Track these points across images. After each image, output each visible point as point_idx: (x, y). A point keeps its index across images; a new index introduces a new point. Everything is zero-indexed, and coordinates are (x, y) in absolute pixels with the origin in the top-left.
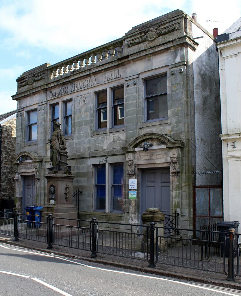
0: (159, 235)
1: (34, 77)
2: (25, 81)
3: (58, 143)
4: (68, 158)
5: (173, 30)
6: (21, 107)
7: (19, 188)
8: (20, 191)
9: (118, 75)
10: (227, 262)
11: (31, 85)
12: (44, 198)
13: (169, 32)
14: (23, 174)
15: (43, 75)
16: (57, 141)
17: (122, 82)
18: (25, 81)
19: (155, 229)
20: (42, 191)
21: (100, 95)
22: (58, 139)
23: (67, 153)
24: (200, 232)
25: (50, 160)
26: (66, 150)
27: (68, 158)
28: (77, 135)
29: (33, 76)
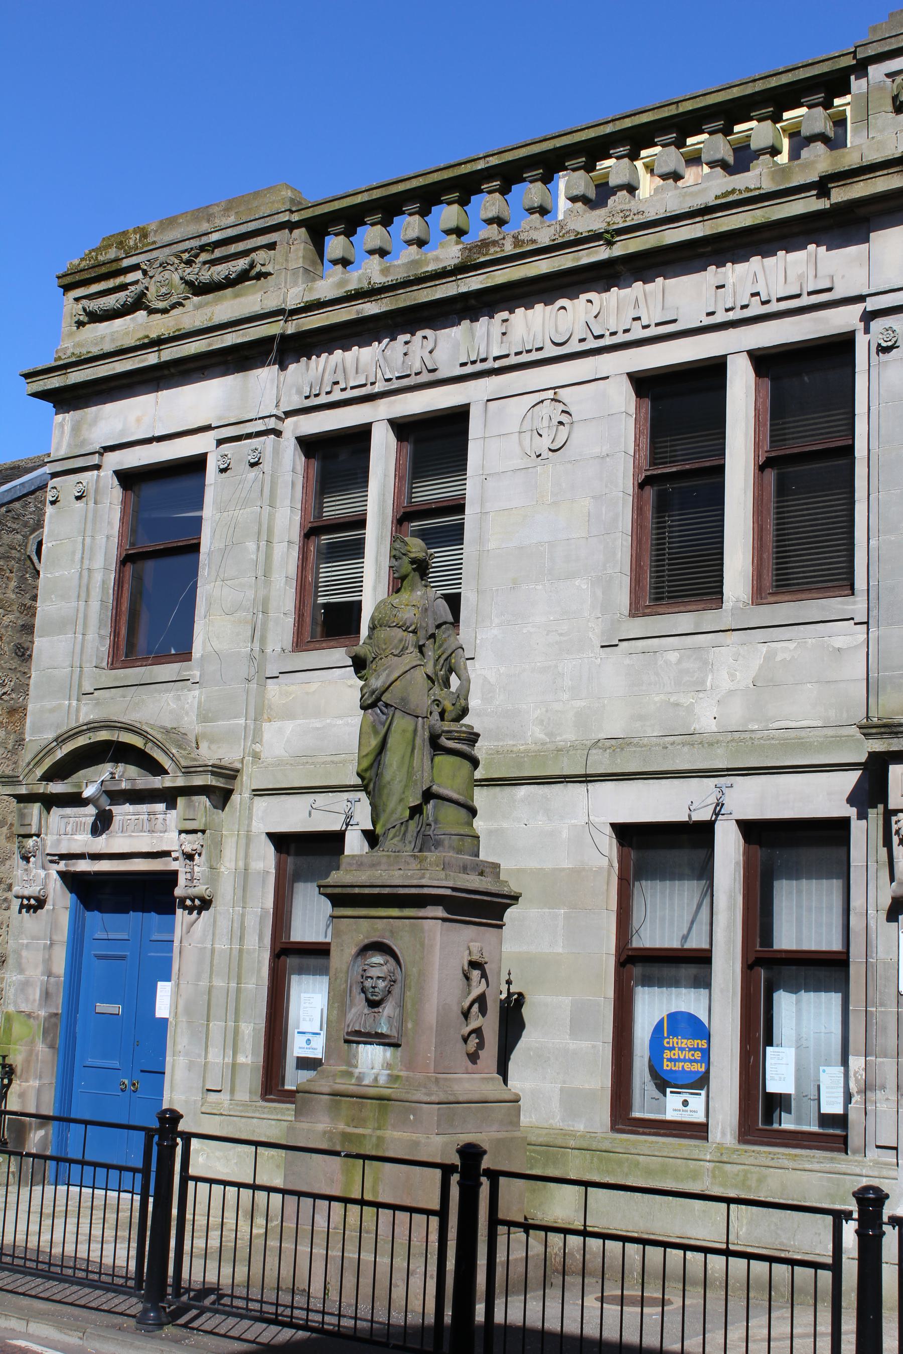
0: (501, 1216)
1: (189, 263)
2: (123, 287)
3: (419, 675)
4: (478, 774)
5: (244, 276)
6: (83, 443)
7: (40, 956)
8: (50, 975)
9: (812, 273)
10: (480, 1309)
11: (165, 311)
12: (231, 1024)
13: (229, 283)
14: (83, 866)
15: (260, 256)
16: (411, 657)
17: (845, 319)
18: (123, 287)
19: (885, 1228)
20: (219, 983)
21: (679, 402)
22: (421, 649)
23: (473, 738)
24: (830, 1218)
25: (359, 781)
26: (466, 721)
27: (478, 774)
28: (495, 631)
29: (185, 256)
